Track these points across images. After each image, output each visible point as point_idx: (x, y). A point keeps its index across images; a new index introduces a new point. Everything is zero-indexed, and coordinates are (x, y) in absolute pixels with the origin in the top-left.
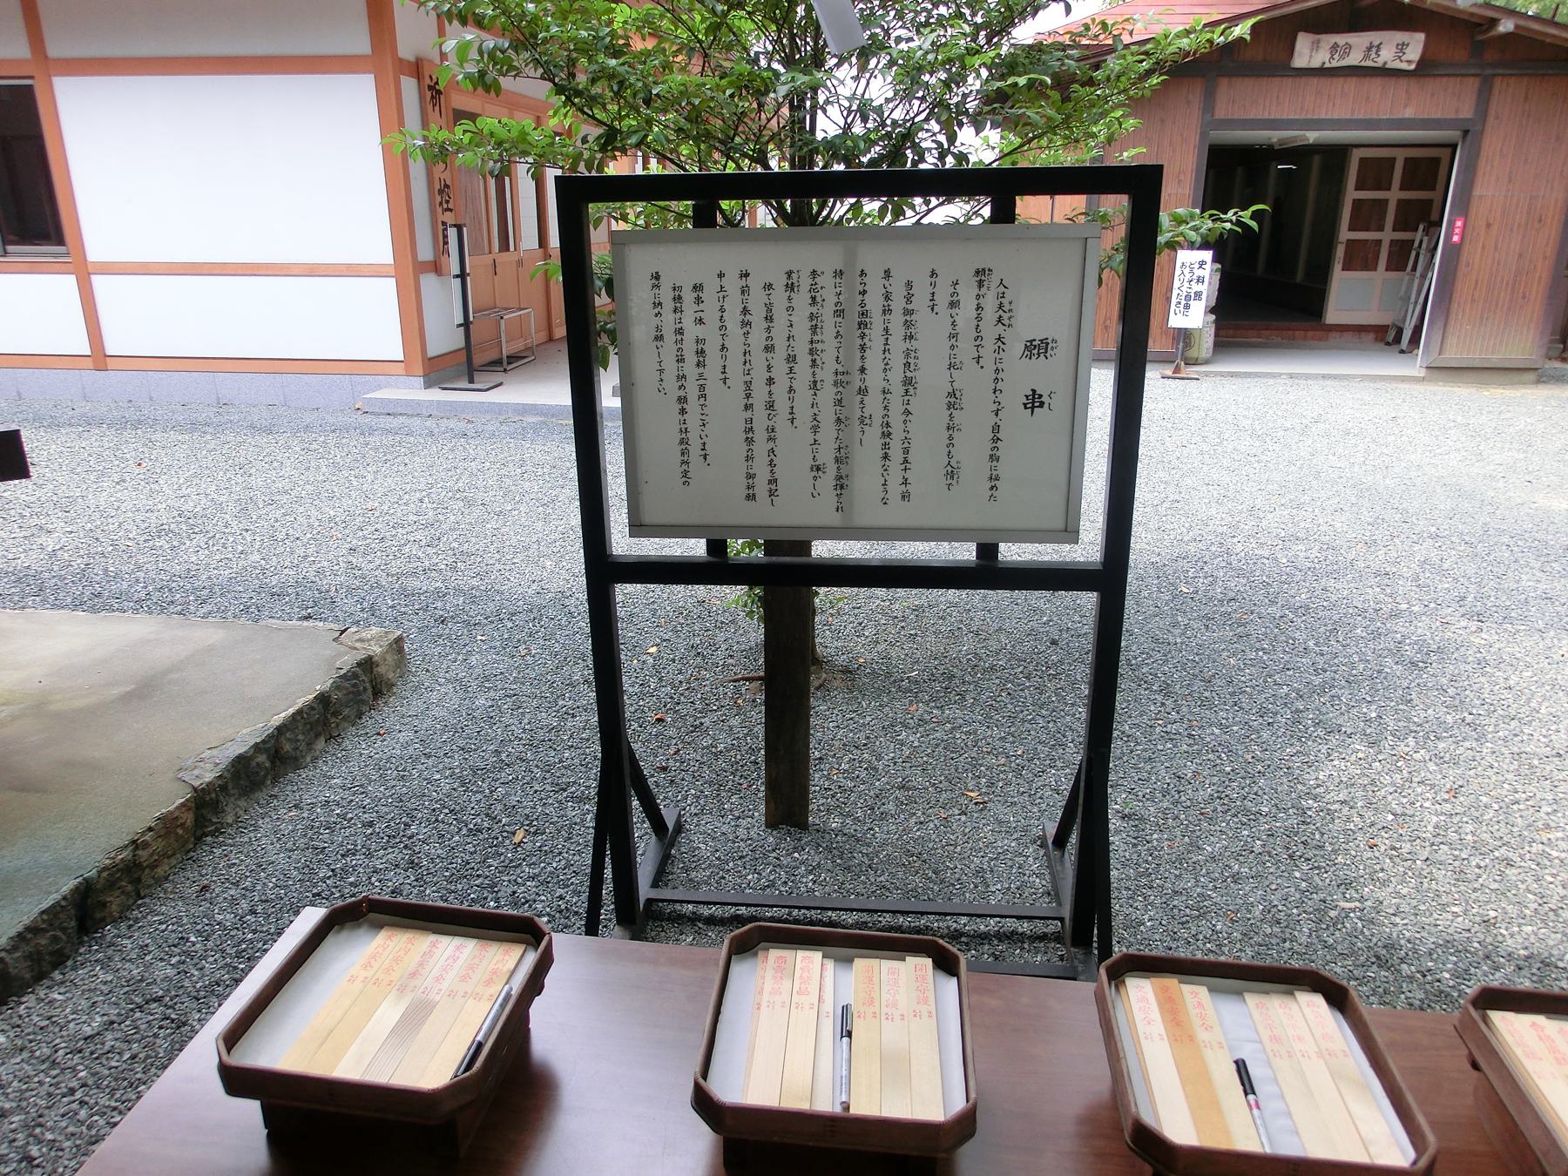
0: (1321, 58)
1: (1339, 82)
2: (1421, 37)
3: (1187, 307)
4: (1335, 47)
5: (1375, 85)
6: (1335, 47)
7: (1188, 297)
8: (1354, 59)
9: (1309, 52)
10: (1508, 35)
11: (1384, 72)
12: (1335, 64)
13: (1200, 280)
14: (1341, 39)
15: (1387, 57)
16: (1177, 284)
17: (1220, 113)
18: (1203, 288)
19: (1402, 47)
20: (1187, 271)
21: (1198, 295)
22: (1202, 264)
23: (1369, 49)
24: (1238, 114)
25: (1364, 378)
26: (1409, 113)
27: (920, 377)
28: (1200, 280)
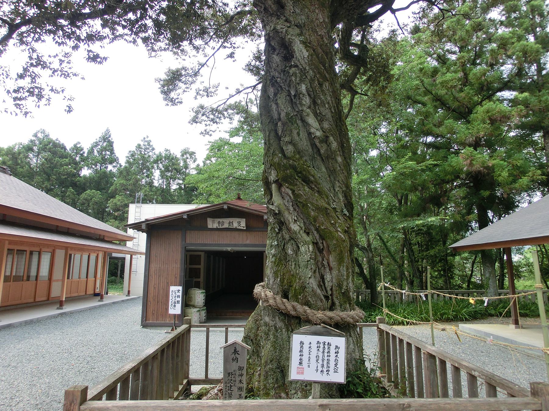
0: (215, 226)
1: (225, 233)
2: (244, 220)
3: (175, 306)
4: (219, 222)
5: (236, 233)
6: (219, 222)
7: (175, 303)
8: (226, 226)
9: (212, 224)
10: (545, 75)
11: (236, 230)
12: (221, 227)
13: (178, 296)
14: (221, 220)
15: (235, 225)
16: (170, 298)
17: (188, 241)
18: (180, 299)
19: (239, 223)
20: (174, 293)
21: (178, 302)
22: (179, 291)
23: (230, 223)
24: (193, 242)
25: (27, 323)
26: (248, 242)
27: (331, 265)
28: (178, 296)
